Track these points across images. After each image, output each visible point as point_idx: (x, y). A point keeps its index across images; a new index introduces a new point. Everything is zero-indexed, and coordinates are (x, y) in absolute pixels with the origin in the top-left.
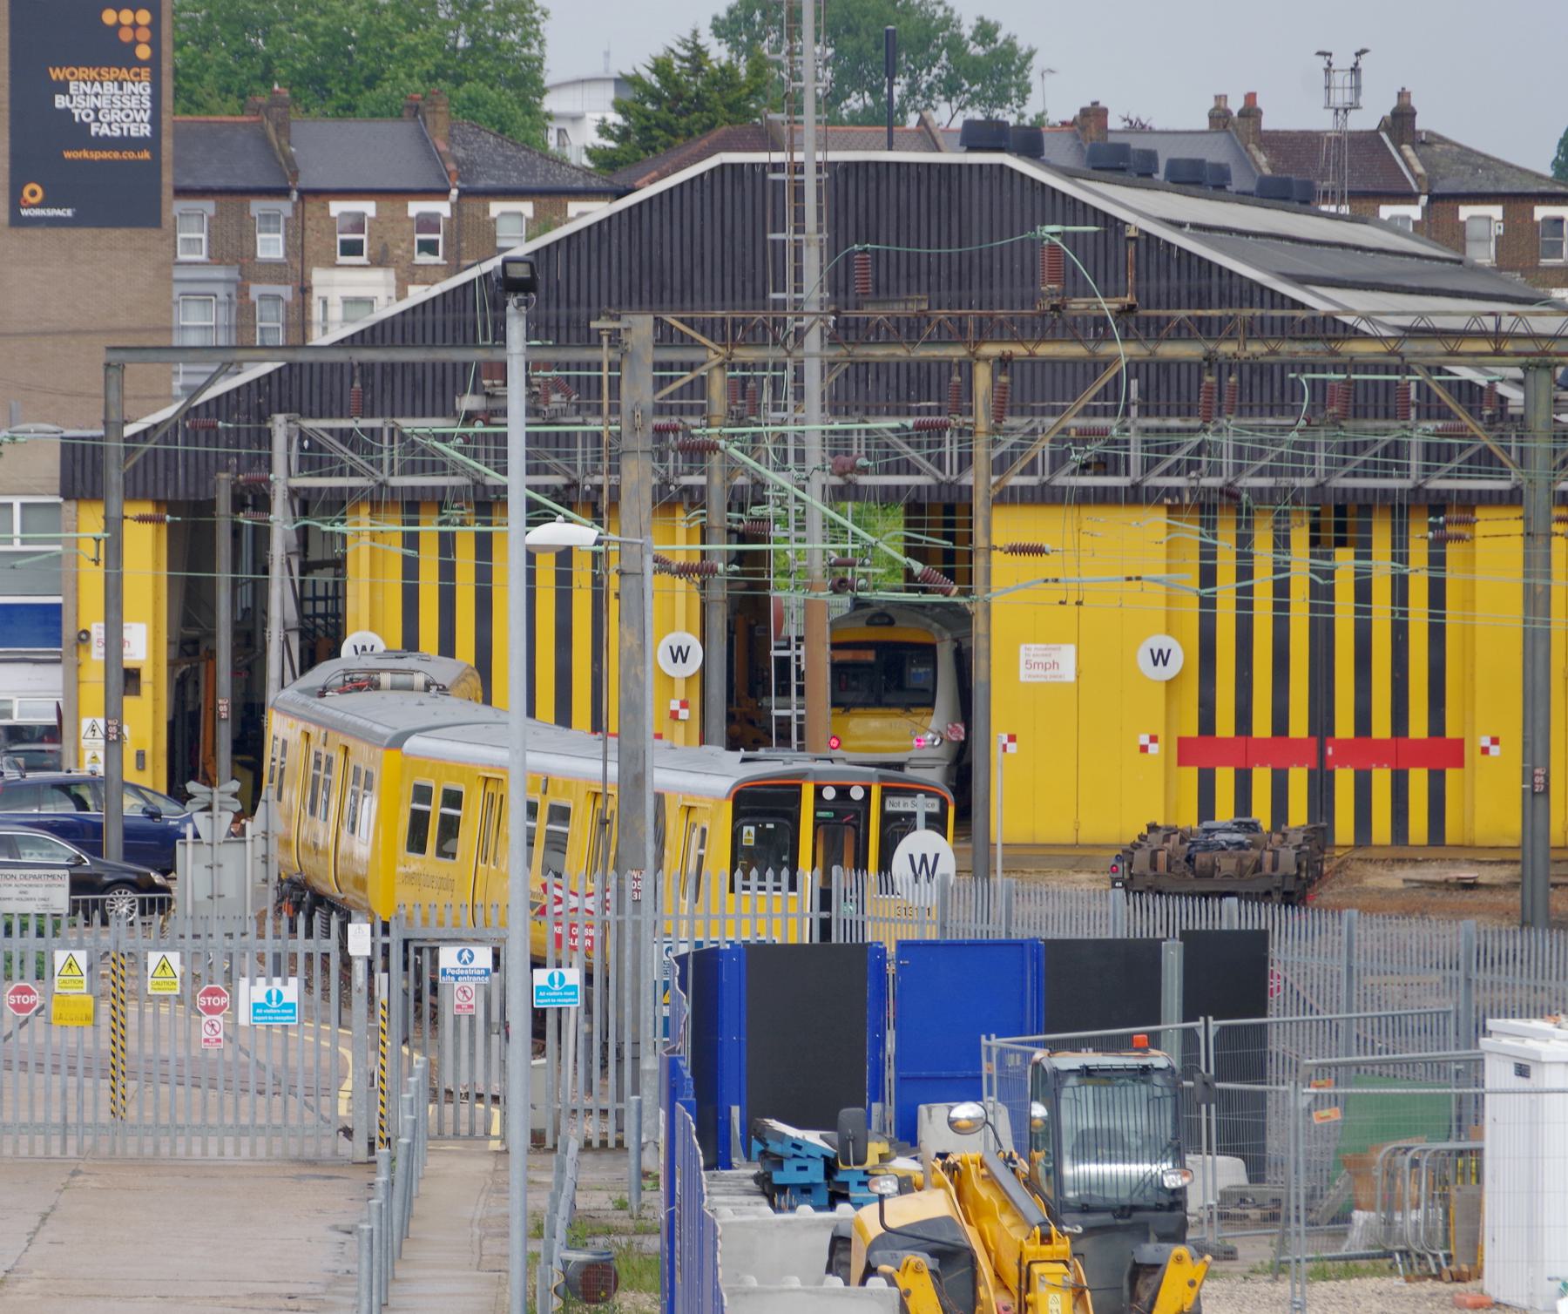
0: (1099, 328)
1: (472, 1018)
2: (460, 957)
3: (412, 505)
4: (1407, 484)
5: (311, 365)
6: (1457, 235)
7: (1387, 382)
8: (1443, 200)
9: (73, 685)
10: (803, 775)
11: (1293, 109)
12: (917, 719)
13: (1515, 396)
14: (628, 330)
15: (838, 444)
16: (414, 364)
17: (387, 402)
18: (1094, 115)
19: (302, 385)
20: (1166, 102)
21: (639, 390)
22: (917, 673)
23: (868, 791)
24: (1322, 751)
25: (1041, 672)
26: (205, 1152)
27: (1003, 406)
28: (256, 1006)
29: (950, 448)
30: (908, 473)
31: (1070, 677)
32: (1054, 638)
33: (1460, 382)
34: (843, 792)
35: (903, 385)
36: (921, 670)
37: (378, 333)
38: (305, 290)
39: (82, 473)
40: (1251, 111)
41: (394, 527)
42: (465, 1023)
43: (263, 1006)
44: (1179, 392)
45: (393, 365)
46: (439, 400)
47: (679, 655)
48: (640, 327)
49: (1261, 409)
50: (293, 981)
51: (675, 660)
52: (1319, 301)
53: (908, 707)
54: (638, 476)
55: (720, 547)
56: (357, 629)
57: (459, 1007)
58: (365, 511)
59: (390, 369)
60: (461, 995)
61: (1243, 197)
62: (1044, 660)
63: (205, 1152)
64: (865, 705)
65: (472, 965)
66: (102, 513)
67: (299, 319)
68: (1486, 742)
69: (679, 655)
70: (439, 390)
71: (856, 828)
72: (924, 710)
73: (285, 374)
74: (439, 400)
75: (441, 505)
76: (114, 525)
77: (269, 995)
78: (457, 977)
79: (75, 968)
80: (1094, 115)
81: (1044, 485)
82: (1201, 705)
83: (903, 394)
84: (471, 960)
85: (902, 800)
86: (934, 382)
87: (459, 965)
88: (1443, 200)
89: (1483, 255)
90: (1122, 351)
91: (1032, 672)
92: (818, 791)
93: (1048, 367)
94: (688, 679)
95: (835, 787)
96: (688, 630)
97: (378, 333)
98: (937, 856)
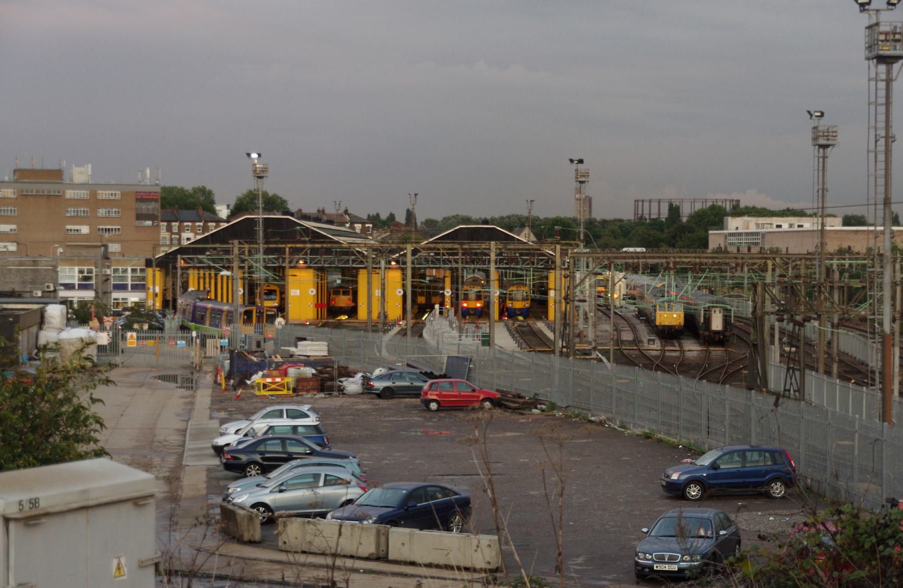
0: (304, 242)
3: (199, 268)
6: (354, 228)
8: (352, 223)
9: (147, 295)
11: (330, 210)
13: (366, 253)
15: (264, 260)
18: (300, 210)
19: (182, 251)
20: (310, 209)
21: (236, 251)
27: (291, 254)
29: (281, 260)
32: (296, 289)
38: (180, 236)
39: (149, 263)
40: (323, 211)
41: (196, 272)
48: (236, 242)
52: (336, 238)
54: (235, 265)
55: (246, 275)
61: (324, 223)
66: (730, 218)
67: (179, 240)
76: (154, 271)
80: (300, 210)
88: (352, 223)
89: (358, 231)
90: (309, 246)
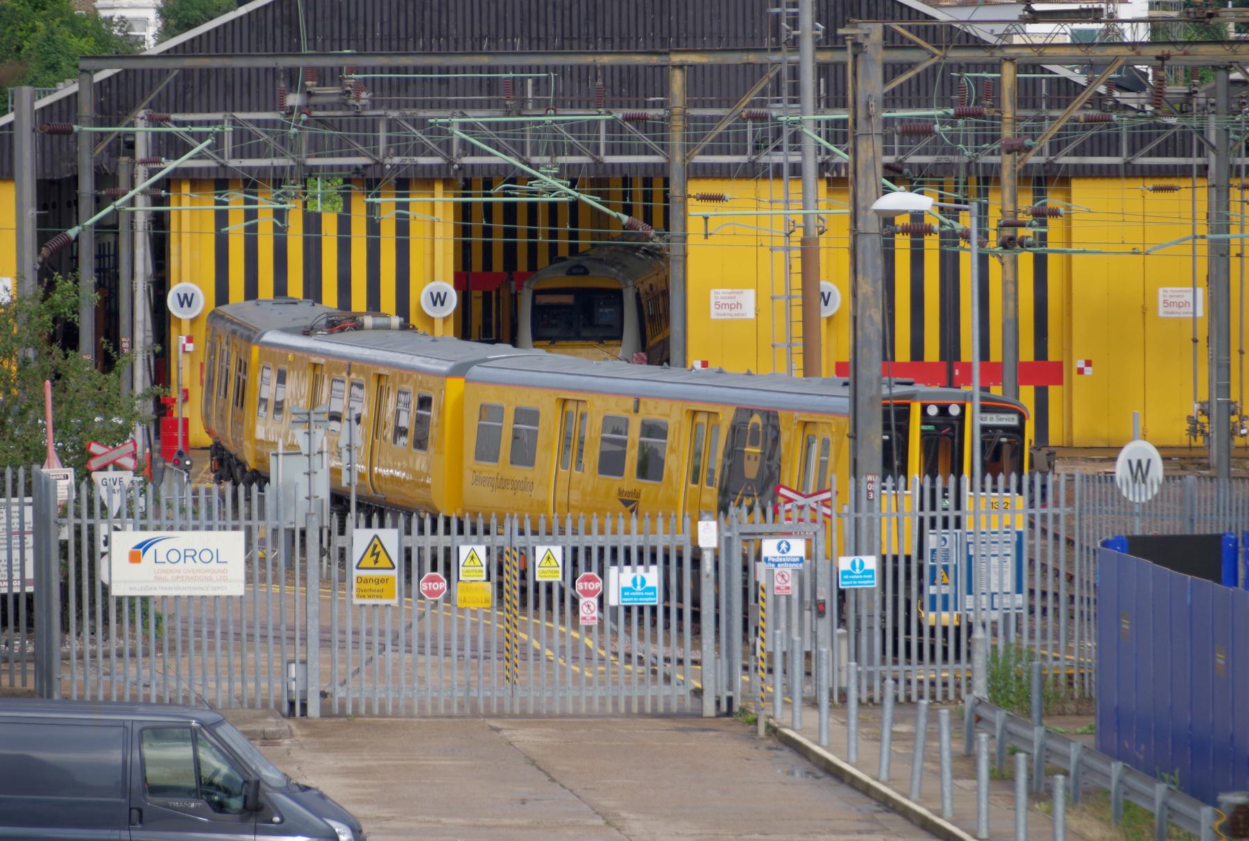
1: (789, 598)
2: (779, 548)
4: (1042, 160)
5: (143, 71)
7: (1034, 79)
10: (912, 396)
12: (610, 349)
14: (867, 36)
16: (225, 69)
17: (204, 100)
22: (605, 313)
23: (963, 408)
24: (951, 372)
25: (727, 311)
26: (12, 684)
28: (624, 590)
30: (646, 154)
31: (751, 315)
32: (738, 284)
33: (1059, 79)
34: (943, 410)
35: (616, 83)
36: (607, 310)
37: (196, 45)
42: (783, 601)
43: (629, 589)
44: (836, 88)
45: (208, 70)
46: (245, 98)
47: (186, 301)
49: (893, 101)
50: (653, 568)
51: (435, 304)
53: (601, 340)
56: (180, 281)
57: (778, 588)
58: (186, 188)
59: (205, 73)
60: (780, 579)
62: (730, 301)
63: (12, 684)
64: (568, 339)
65: (791, 553)
68: (1081, 364)
69: (439, 299)
70: (245, 89)
71: (953, 438)
72: (614, 342)
73: (122, 78)
74: (245, 98)
75: (278, 183)
77: (634, 581)
78: (776, 564)
79: (383, 560)
81: (753, 163)
82: (1046, 335)
83: (616, 91)
84: (788, 549)
85: (994, 416)
86: (641, 81)
87: (778, 554)
91: (720, 311)
92: (924, 409)
93: (657, 70)
94: (445, 319)
95: (937, 405)
96: (445, 280)
97: (196, 45)
98: (1149, 461)
